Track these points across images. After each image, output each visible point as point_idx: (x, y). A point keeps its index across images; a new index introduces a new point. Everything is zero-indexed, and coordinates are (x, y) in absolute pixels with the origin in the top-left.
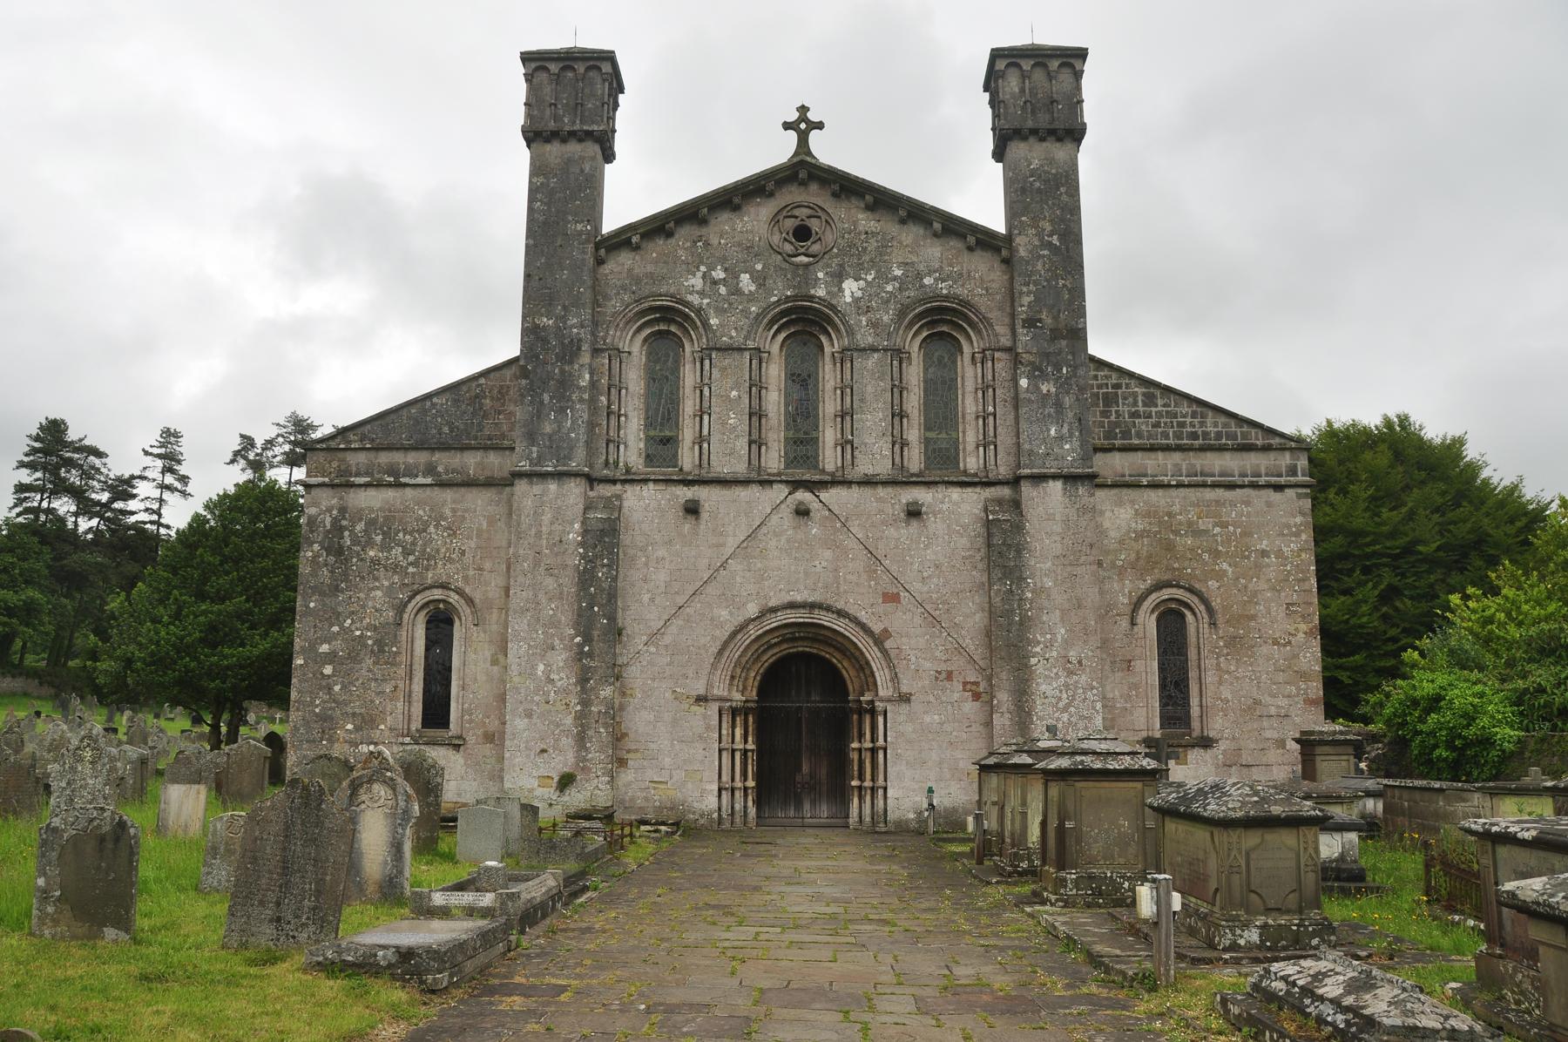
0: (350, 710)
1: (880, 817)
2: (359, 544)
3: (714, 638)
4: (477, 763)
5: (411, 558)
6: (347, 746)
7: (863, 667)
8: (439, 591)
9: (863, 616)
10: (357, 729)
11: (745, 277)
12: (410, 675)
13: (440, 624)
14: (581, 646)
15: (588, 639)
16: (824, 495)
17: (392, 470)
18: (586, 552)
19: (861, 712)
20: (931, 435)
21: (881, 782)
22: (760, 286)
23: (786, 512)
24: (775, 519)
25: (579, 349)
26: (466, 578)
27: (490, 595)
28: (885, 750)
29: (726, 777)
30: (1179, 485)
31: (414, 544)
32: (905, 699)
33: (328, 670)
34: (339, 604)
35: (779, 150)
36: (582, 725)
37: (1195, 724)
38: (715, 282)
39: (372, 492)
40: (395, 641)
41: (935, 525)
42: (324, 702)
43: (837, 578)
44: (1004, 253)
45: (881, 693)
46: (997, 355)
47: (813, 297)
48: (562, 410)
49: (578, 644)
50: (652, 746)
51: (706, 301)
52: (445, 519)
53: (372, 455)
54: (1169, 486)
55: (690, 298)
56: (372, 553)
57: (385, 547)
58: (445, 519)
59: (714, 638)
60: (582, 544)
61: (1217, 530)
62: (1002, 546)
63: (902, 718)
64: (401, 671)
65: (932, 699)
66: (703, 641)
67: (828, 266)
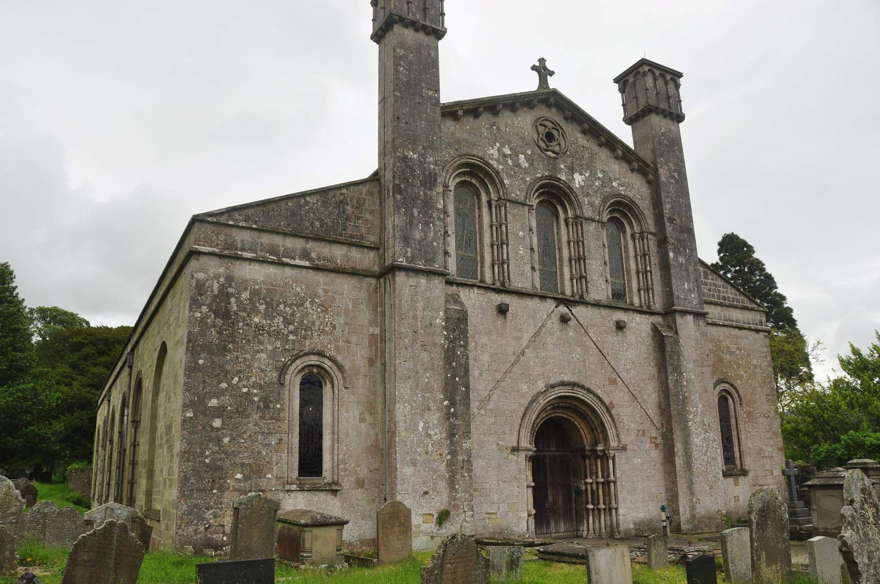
0: (238, 461)
2: (244, 310)
4: (352, 506)
5: (291, 327)
6: (236, 494)
8: (316, 358)
9: (599, 392)
10: (246, 478)
11: (522, 157)
12: (290, 428)
13: (313, 385)
14: (448, 408)
15: (453, 403)
16: (574, 310)
17: (273, 251)
18: (449, 335)
22: (531, 165)
23: (555, 319)
25: (436, 180)
26: (337, 348)
27: (357, 363)
28: (615, 482)
30: (724, 325)
31: (293, 315)
32: (624, 448)
33: (217, 423)
34: (227, 362)
35: (530, 84)
36: (452, 471)
37: (738, 462)
38: (505, 156)
39: (255, 267)
40: (279, 399)
41: (630, 334)
42: (213, 453)
43: (585, 366)
44: (651, 177)
46: (650, 236)
47: (560, 179)
48: (427, 224)
49: (446, 406)
50: (486, 486)
51: (501, 167)
52: (319, 298)
53: (255, 235)
54: (719, 325)
55: (491, 162)
56: (256, 320)
57: (266, 316)
58: (319, 298)
60: (445, 328)
61: (738, 352)
62: (664, 349)
63: (623, 461)
64: (285, 427)
65: (637, 448)
67: (566, 162)
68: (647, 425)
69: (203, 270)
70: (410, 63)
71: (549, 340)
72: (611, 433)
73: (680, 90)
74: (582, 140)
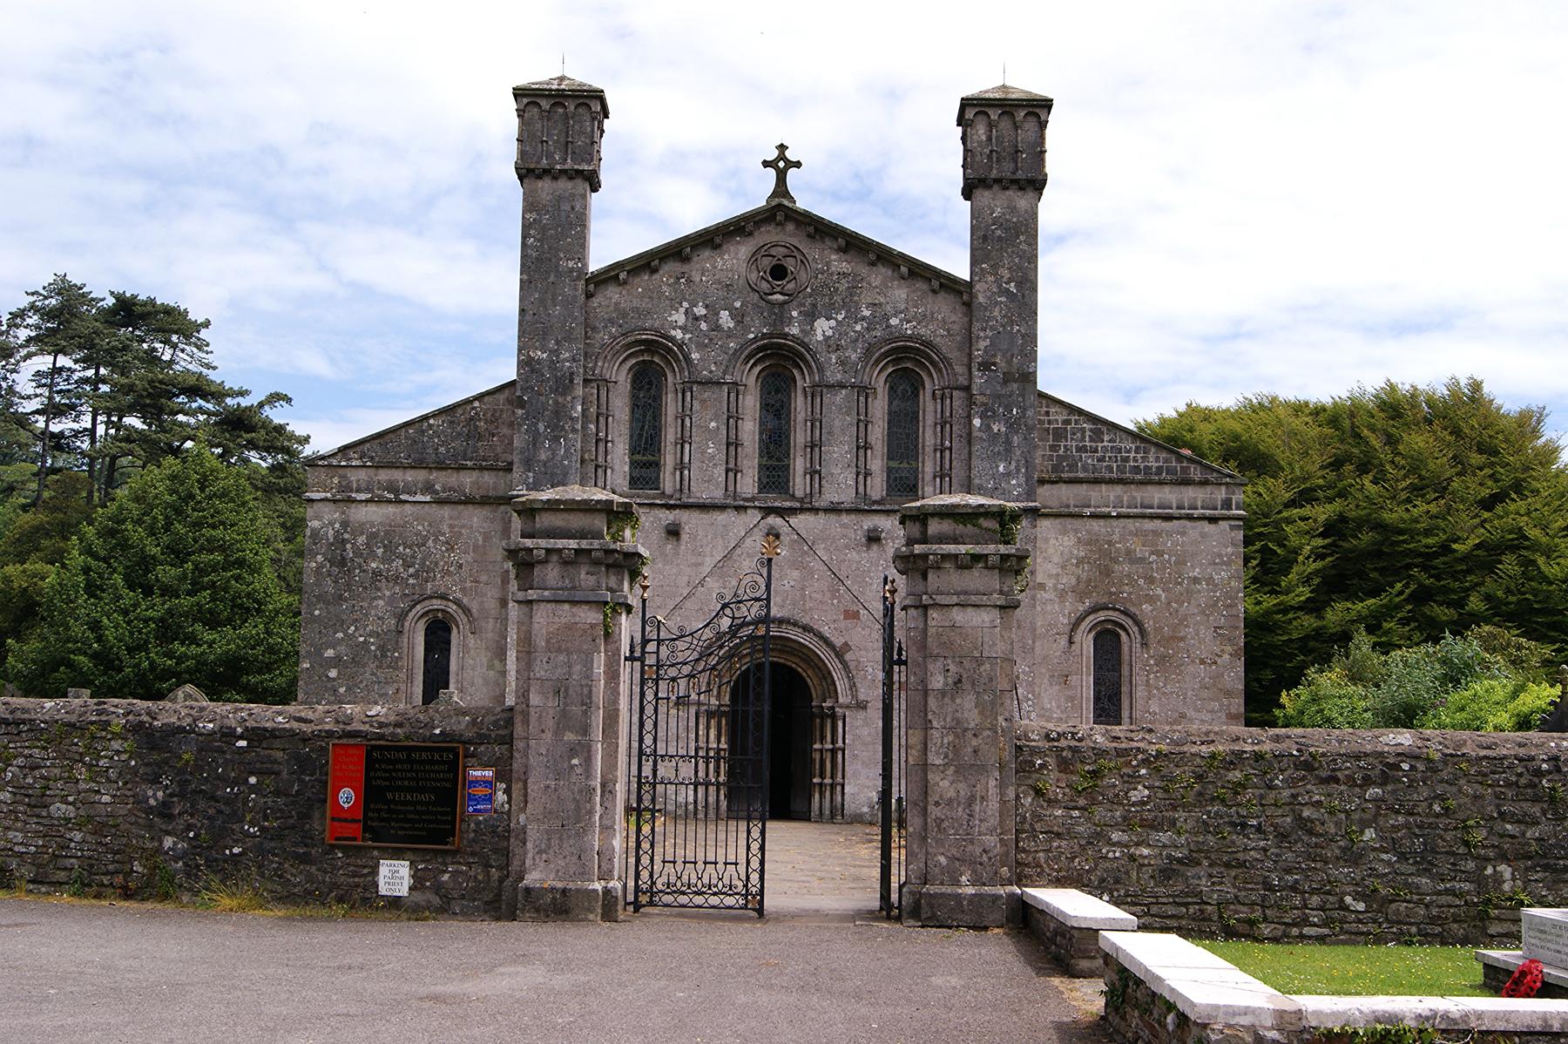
5: (411, 570)
7: (826, 676)
9: (826, 631)
11: (724, 314)
13: (439, 634)
19: (823, 716)
22: (738, 323)
24: (748, 541)
30: (1119, 516)
31: (413, 557)
33: (333, 673)
38: (696, 319)
39: (372, 508)
43: (803, 597)
45: (841, 700)
48: (556, 439)
53: (371, 472)
54: (1107, 516)
55: (673, 333)
63: (859, 723)
70: (544, 229)
73: (1049, 132)
74: (840, 263)
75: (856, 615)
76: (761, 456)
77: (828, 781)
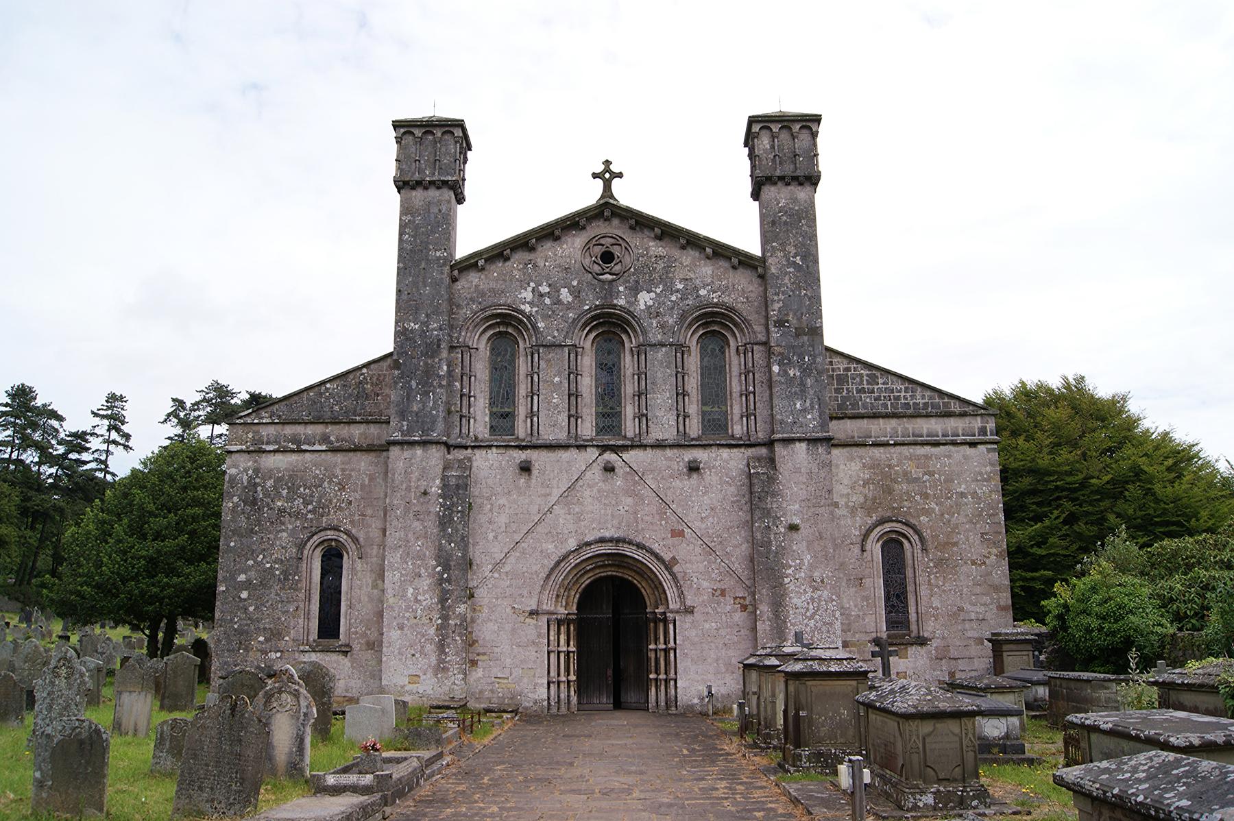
1: (671, 702)
3: (543, 566)
5: (310, 507)
6: (259, 654)
7: (658, 586)
8: (332, 532)
9: (656, 548)
11: (564, 291)
13: (333, 559)
14: (441, 574)
16: (625, 456)
17: (295, 440)
20: (705, 408)
21: (672, 675)
22: (576, 297)
23: (596, 473)
24: (589, 474)
28: (675, 650)
29: (553, 673)
30: (895, 445)
31: (312, 496)
32: (689, 611)
33: (244, 595)
35: (590, 194)
37: (913, 627)
39: (279, 457)
41: (710, 477)
43: (636, 519)
48: (426, 394)
51: (535, 309)
53: (279, 427)
55: (522, 307)
56: (279, 504)
59: (543, 566)
62: (758, 493)
63: (688, 625)
66: (535, 568)
68: (729, 583)
69: (235, 466)
70: (417, 228)
71: (587, 493)
72: (671, 594)
73: (819, 140)
75: (681, 534)
76: (597, 405)
77: (662, 676)
